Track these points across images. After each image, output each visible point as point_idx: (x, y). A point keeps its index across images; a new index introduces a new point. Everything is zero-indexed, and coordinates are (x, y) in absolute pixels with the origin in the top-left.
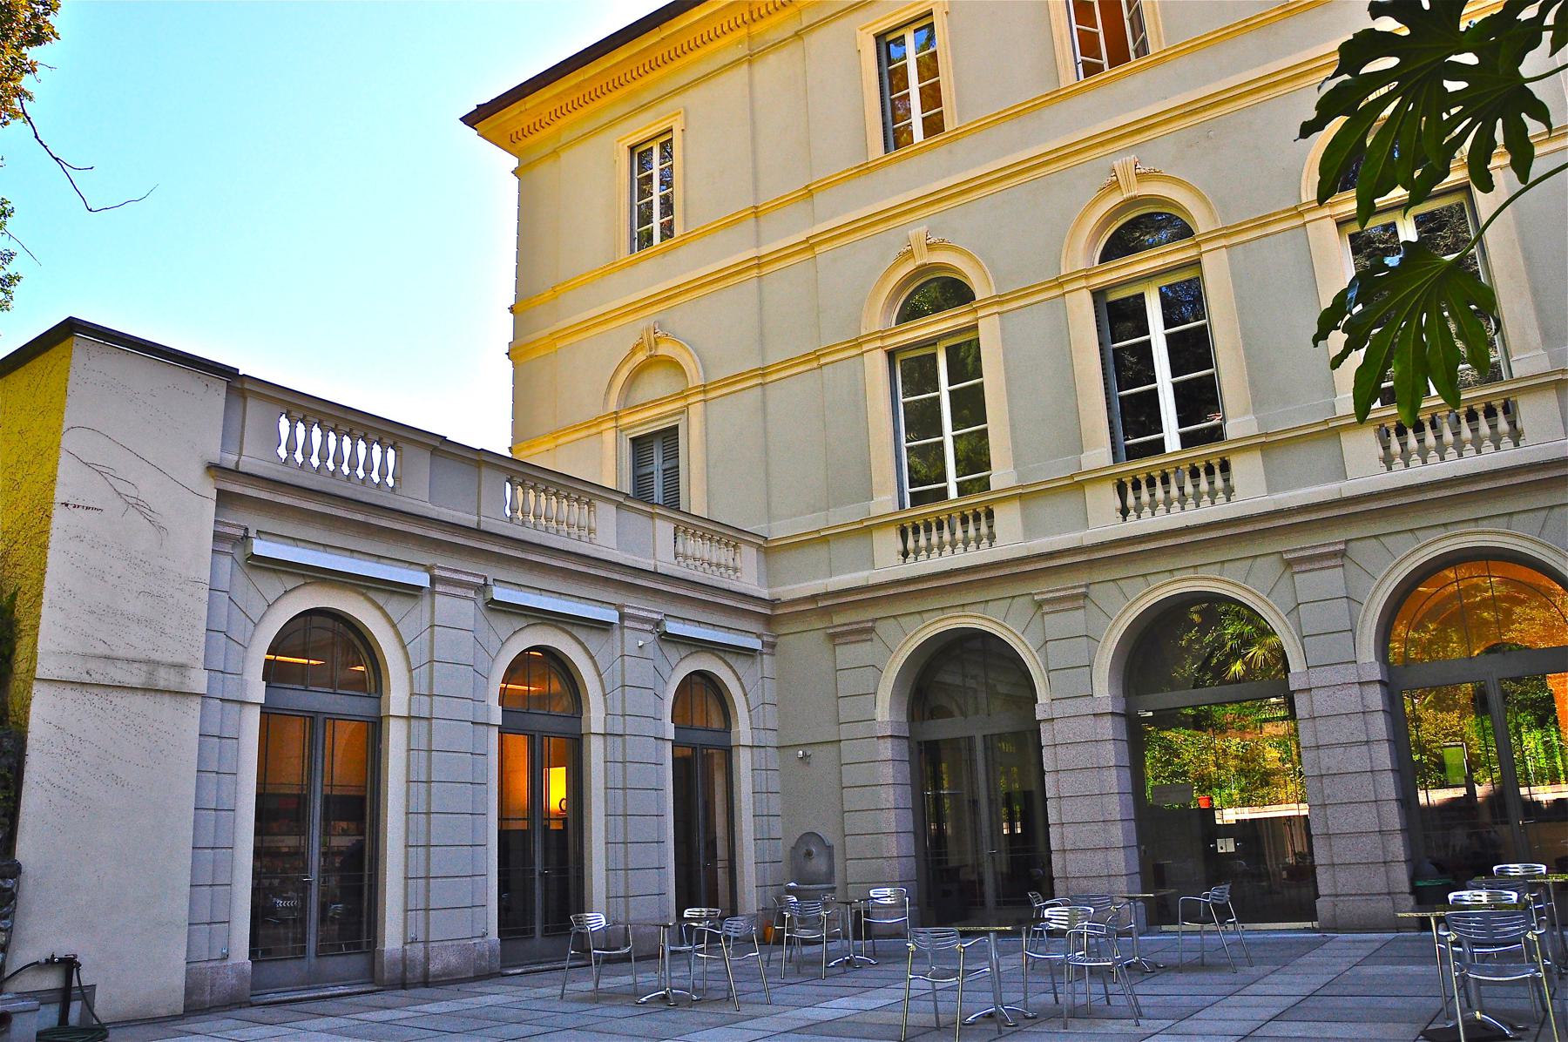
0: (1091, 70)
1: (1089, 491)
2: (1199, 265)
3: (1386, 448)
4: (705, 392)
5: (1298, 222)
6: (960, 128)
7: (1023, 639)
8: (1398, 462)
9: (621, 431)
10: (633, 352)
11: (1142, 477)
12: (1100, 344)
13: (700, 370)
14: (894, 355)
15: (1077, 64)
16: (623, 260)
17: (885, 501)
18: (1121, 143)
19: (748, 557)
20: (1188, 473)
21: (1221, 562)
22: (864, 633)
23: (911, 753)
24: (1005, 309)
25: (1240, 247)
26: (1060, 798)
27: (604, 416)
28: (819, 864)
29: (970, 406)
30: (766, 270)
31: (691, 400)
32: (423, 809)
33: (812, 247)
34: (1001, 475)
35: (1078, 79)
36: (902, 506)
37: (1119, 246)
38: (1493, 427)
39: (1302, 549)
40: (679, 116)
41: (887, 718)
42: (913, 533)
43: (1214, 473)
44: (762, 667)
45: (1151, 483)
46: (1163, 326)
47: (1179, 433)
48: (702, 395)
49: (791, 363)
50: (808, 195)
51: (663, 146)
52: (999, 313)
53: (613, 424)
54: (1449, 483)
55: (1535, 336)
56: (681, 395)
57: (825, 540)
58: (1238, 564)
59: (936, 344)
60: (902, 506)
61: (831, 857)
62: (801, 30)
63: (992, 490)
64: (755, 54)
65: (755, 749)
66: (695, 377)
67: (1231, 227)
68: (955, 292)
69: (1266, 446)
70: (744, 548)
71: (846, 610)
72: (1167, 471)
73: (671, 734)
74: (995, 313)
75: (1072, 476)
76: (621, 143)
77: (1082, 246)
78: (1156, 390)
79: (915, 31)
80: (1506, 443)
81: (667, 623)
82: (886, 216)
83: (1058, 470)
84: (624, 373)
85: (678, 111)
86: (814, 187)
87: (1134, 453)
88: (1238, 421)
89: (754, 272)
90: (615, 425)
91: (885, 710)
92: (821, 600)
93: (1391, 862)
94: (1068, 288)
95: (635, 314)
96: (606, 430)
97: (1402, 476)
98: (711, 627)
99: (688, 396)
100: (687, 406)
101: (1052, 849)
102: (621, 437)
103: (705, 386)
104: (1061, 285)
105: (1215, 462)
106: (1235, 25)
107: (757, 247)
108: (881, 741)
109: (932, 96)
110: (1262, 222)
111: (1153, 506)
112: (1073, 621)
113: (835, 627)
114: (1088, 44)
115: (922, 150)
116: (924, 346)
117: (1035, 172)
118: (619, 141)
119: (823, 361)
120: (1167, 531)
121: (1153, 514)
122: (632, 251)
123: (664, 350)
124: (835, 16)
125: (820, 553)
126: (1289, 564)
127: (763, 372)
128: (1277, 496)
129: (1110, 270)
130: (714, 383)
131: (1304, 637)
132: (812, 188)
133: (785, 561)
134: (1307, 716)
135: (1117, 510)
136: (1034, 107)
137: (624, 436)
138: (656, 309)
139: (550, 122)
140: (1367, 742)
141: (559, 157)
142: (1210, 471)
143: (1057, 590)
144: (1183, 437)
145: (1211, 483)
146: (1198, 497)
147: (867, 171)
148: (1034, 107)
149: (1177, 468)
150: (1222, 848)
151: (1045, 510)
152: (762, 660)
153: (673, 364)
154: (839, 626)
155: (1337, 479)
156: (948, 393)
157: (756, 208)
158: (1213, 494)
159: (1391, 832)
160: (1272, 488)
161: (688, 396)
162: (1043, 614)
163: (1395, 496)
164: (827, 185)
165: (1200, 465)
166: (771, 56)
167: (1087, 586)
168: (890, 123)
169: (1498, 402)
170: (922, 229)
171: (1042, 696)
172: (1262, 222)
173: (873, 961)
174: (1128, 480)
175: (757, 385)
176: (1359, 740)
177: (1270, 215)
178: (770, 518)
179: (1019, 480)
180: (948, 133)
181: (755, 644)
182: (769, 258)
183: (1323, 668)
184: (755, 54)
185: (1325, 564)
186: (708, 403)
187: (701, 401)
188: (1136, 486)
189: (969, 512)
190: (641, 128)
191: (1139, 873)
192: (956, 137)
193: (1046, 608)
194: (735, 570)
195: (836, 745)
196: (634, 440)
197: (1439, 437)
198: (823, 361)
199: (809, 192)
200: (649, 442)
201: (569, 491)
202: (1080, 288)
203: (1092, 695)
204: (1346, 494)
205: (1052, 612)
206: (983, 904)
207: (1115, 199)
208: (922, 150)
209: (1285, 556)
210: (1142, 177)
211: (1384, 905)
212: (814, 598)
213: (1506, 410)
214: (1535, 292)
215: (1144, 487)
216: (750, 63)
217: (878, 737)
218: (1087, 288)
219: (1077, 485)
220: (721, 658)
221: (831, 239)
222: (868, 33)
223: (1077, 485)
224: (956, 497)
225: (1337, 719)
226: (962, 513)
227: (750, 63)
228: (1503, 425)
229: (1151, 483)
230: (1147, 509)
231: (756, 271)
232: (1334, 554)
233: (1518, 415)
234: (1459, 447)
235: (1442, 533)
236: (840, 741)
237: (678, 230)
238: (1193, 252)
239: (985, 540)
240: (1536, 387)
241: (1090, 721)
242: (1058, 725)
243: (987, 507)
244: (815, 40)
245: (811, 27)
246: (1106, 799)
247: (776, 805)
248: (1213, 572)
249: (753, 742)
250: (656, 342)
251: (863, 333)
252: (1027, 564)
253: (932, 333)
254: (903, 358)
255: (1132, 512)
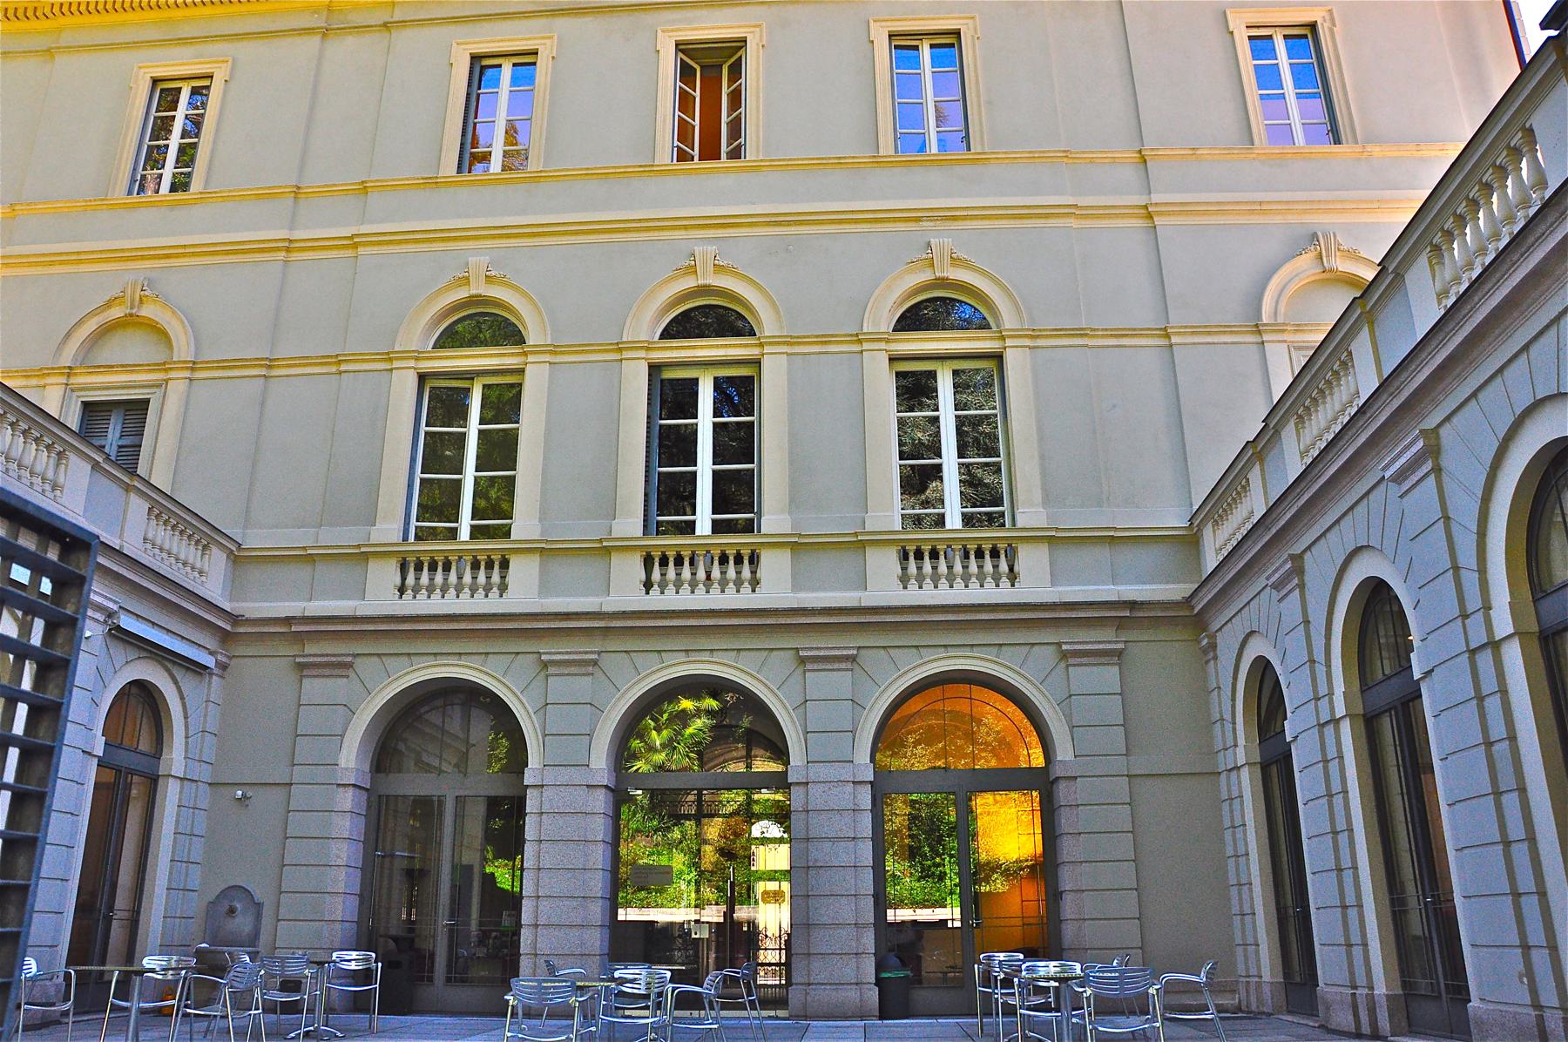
0: (683, 157)
1: (616, 559)
2: (758, 365)
3: (904, 569)
4: (192, 369)
5: (617, 356)
6: (545, 171)
7: (521, 697)
8: (913, 582)
9: (72, 390)
10: (109, 304)
11: (671, 554)
12: (648, 417)
13: (192, 345)
14: (425, 379)
15: (673, 147)
16: (117, 199)
17: (389, 529)
18: (592, 237)
19: (217, 562)
20: (469, 564)
21: (738, 650)
22: (342, 667)
23: (369, 807)
24: (557, 361)
25: (800, 357)
26: (539, 869)
27: (53, 369)
28: (242, 923)
29: (500, 451)
30: (295, 256)
31: (173, 374)
32: (544, 816)
33: (355, 246)
34: (524, 524)
35: (672, 161)
36: (405, 538)
37: (684, 326)
38: (996, 567)
39: (817, 648)
40: (226, 64)
41: (352, 765)
42: (735, 564)
43: (479, 569)
44: (209, 689)
45: (679, 561)
46: (712, 415)
47: (471, 526)
48: (644, 352)
49: (305, 361)
50: (361, 192)
51: (195, 91)
52: (550, 363)
53: (63, 380)
54: (956, 609)
55: (1038, 495)
56: (163, 366)
57: (311, 559)
58: (502, 656)
59: (473, 379)
60: (405, 538)
61: (258, 916)
62: (391, 23)
63: (697, 534)
64: (332, 30)
65: (186, 782)
66: (183, 348)
67: (795, 337)
68: (506, 332)
69: (797, 546)
70: (215, 550)
71: (417, 638)
72: (436, 558)
73: (99, 751)
74: (783, 353)
75: (600, 541)
76: (142, 70)
77: (648, 319)
78: (694, 474)
79: (514, 65)
80: (1005, 582)
81: (122, 617)
82: (447, 236)
83: (586, 531)
84: (91, 326)
85: (226, 59)
86: (372, 185)
87: (662, 529)
88: (774, 518)
89: (281, 255)
90: (65, 382)
91: (351, 757)
92: (296, 624)
93: (863, 953)
94: (626, 354)
95: (122, 263)
96: (52, 384)
97: (657, 600)
98: (179, 639)
99: (171, 369)
100: (167, 381)
101: (523, 923)
102: (70, 398)
103: (194, 363)
104: (620, 350)
105: (496, 557)
106: (830, 158)
107: (291, 230)
108: (341, 789)
109: (187, 155)
110: (825, 340)
111: (678, 585)
112: (581, 686)
113: (307, 656)
114: (684, 132)
115: (496, 181)
116: (461, 379)
117: (614, 236)
118: (140, 68)
119: (343, 367)
120: (692, 611)
121: (677, 592)
122: (130, 193)
123: (147, 311)
124: (432, 21)
125: (302, 573)
126: (1065, 655)
127: (270, 363)
128: (802, 595)
129: (671, 348)
130: (207, 362)
131: (808, 732)
132: (367, 185)
133: (255, 574)
134: (801, 809)
135: (641, 581)
136: (624, 174)
137: (74, 398)
138: (148, 264)
139: (50, 15)
140: (854, 838)
141: (54, 58)
142: (739, 560)
143: (569, 653)
144: (715, 523)
145: (739, 573)
146: (723, 583)
147: (434, 186)
148: (624, 174)
149: (460, 558)
150: (696, 934)
151: (566, 570)
152: (210, 683)
153: (159, 332)
154: (310, 655)
155: (856, 589)
156: (477, 432)
157: (299, 188)
158: (738, 583)
159: (865, 925)
160: (796, 586)
161: (171, 369)
162: (1067, 666)
163: (911, 613)
164: (383, 187)
165: (731, 552)
166: (350, 37)
167: (599, 653)
168: (468, 145)
169: (483, 557)
170: (485, 259)
171: (534, 760)
172: (825, 340)
173: (339, 1034)
174: (657, 555)
175: (260, 376)
176: (847, 836)
177: (832, 336)
178: (247, 523)
179: (542, 534)
180: (192, 194)
181: (209, 661)
182: (302, 244)
183: (822, 764)
184: (332, 30)
185: (836, 666)
186: (194, 383)
187: (186, 378)
188: (664, 562)
189: (482, 558)
190: (176, 64)
191: (608, 954)
192: (536, 179)
193: (551, 670)
194: (201, 573)
195: (287, 787)
196: (86, 405)
197: (950, 567)
198: (343, 367)
199: (364, 189)
200: (108, 411)
201: (54, 440)
202: (638, 358)
203: (588, 766)
204: (359, 613)
205: (556, 675)
206: (431, 979)
207: (689, 283)
208: (496, 181)
209: (801, 653)
210: (719, 269)
211: (852, 994)
212: (288, 621)
213: (751, 562)
214: (1042, 457)
215: (671, 564)
216: (324, 35)
217: (338, 785)
218: (415, 369)
219: (605, 550)
220: (168, 670)
221: (379, 243)
222: (464, 50)
223: (605, 550)
224: (468, 539)
225: (830, 815)
226: (475, 557)
227: (324, 35)
228: (746, 572)
229: (679, 561)
230: (671, 586)
231: (283, 254)
232: (846, 658)
233: (1016, 561)
234: (966, 579)
235: (942, 653)
236: (292, 784)
237: (196, 185)
238: (755, 351)
239: (495, 589)
240: (1035, 538)
241: (583, 791)
242: (547, 792)
243: (503, 556)
244: (405, 39)
245: (403, 23)
246: (589, 874)
247: (197, 850)
248: (728, 658)
249: (185, 772)
250: (141, 299)
251: (396, 349)
252: (538, 620)
253: (963, 349)
254: (432, 385)
255: (656, 587)
